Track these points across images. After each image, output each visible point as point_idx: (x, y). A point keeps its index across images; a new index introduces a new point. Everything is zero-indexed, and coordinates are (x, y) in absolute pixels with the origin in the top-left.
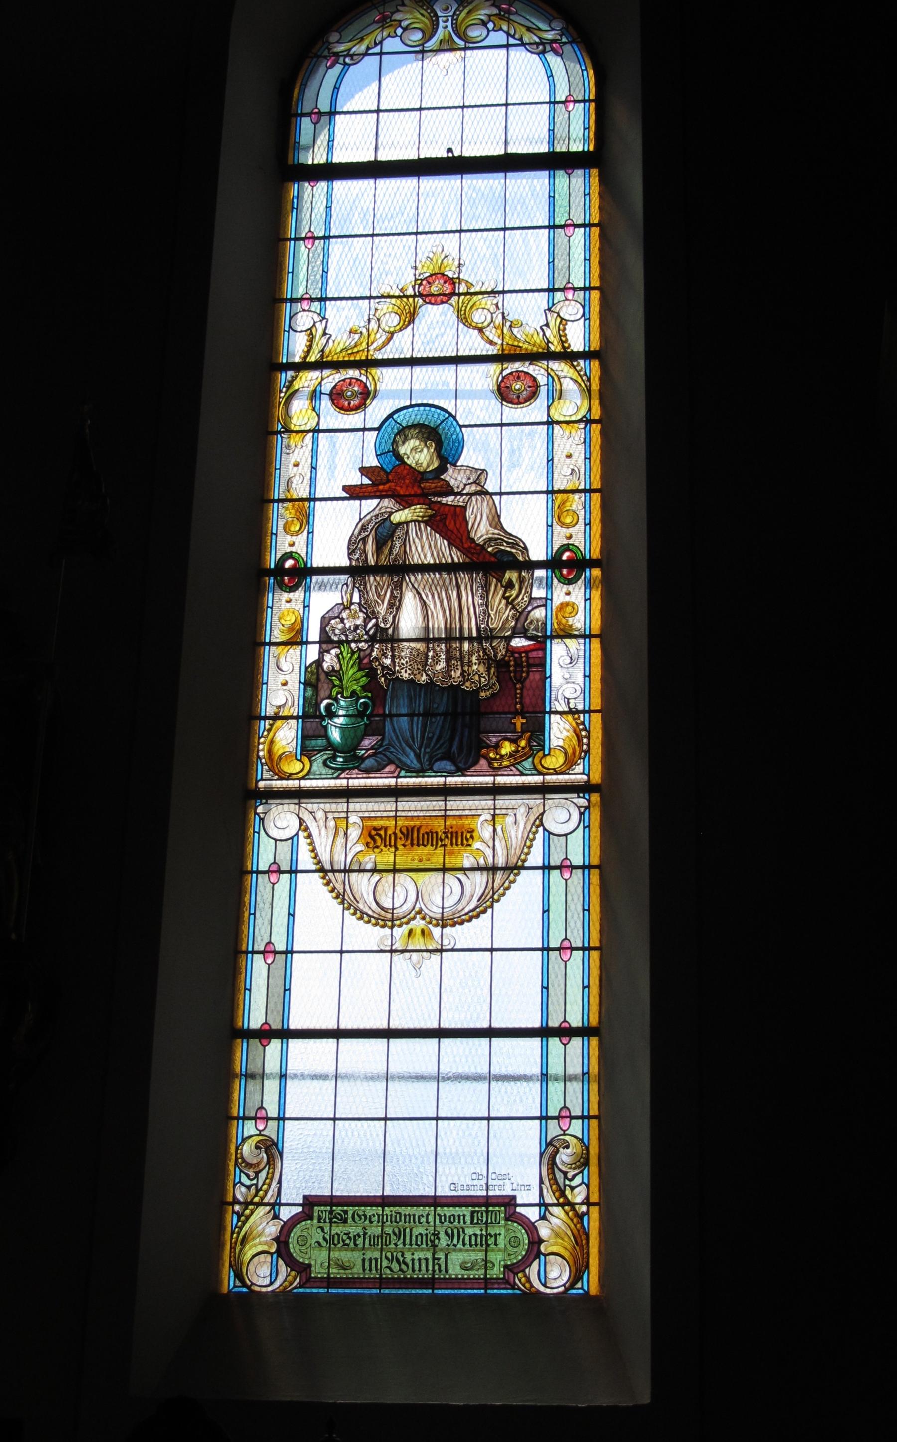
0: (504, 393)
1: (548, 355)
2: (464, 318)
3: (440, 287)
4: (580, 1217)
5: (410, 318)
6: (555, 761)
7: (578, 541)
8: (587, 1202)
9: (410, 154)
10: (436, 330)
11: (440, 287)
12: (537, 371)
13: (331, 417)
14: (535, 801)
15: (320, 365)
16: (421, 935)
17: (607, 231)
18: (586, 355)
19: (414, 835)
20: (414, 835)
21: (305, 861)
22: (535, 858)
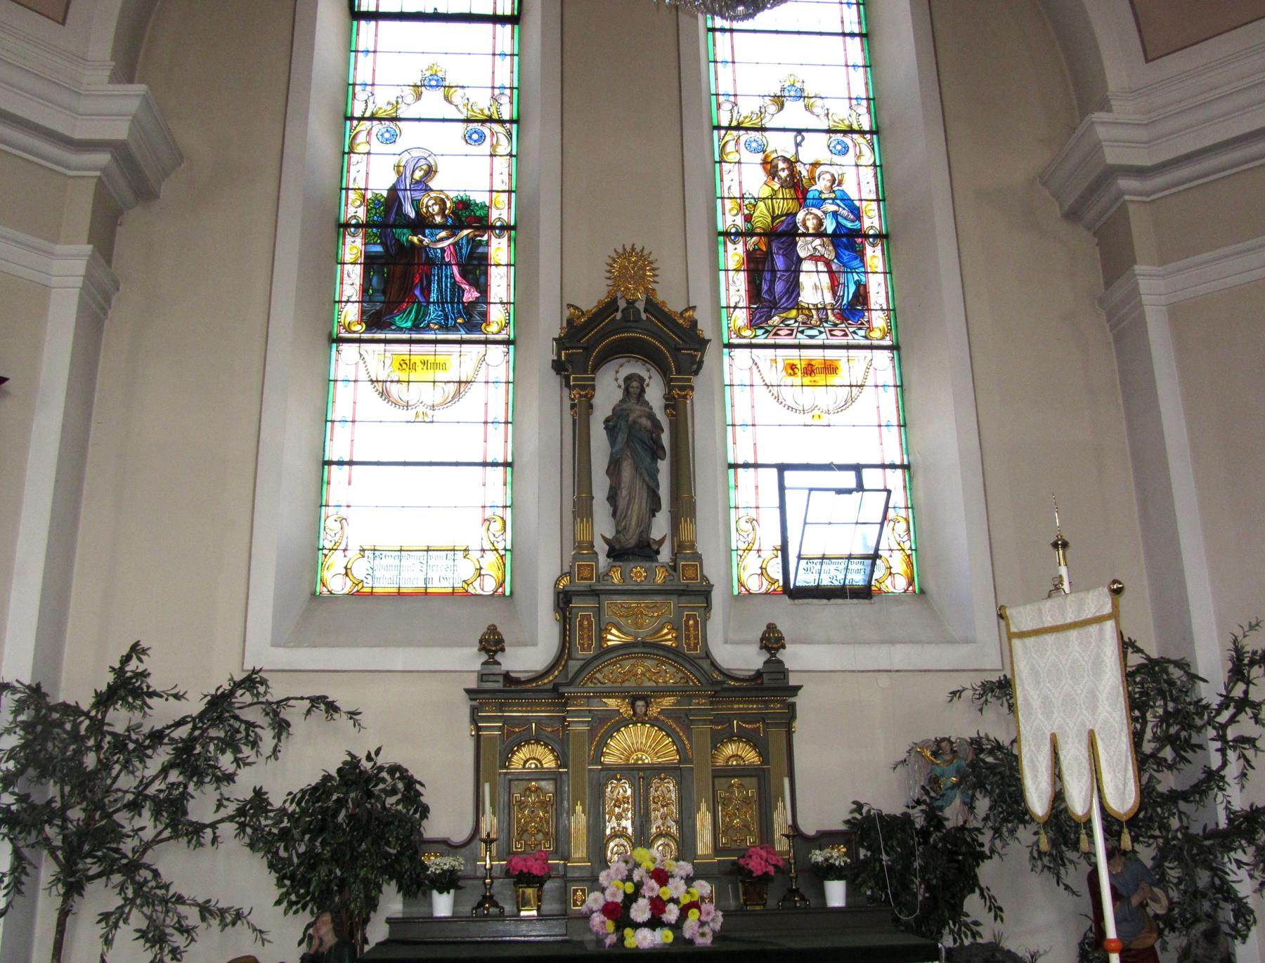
0: (467, 139)
1: (490, 120)
2: (447, 99)
3: (434, 81)
4: (909, 556)
5: (419, 96)
6: (493, 328)
7: (505, 217)
8: (911, 549)
9: (396, 9)
10: (433, 103)
11: (434, 81)
12: (485, 129)
13: (376, 146)
14: (481, 348)
15: (372, 118)
16: (815, 418)
17: (520, 54)
18: (511, 121)
19: (809, 370)
20: (809, 370)
21: (757, 380)
22: (481, 377)
